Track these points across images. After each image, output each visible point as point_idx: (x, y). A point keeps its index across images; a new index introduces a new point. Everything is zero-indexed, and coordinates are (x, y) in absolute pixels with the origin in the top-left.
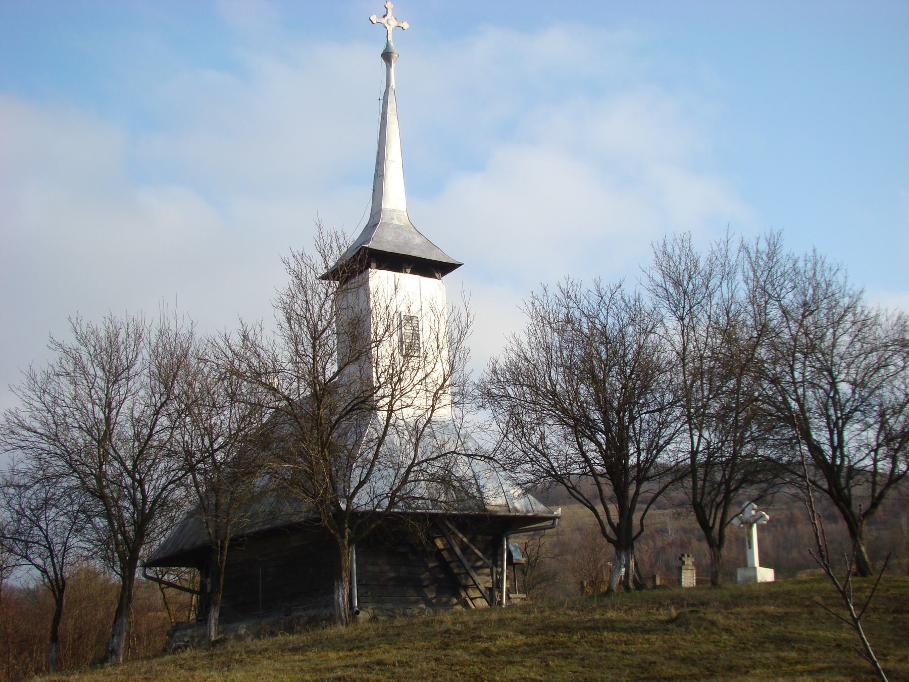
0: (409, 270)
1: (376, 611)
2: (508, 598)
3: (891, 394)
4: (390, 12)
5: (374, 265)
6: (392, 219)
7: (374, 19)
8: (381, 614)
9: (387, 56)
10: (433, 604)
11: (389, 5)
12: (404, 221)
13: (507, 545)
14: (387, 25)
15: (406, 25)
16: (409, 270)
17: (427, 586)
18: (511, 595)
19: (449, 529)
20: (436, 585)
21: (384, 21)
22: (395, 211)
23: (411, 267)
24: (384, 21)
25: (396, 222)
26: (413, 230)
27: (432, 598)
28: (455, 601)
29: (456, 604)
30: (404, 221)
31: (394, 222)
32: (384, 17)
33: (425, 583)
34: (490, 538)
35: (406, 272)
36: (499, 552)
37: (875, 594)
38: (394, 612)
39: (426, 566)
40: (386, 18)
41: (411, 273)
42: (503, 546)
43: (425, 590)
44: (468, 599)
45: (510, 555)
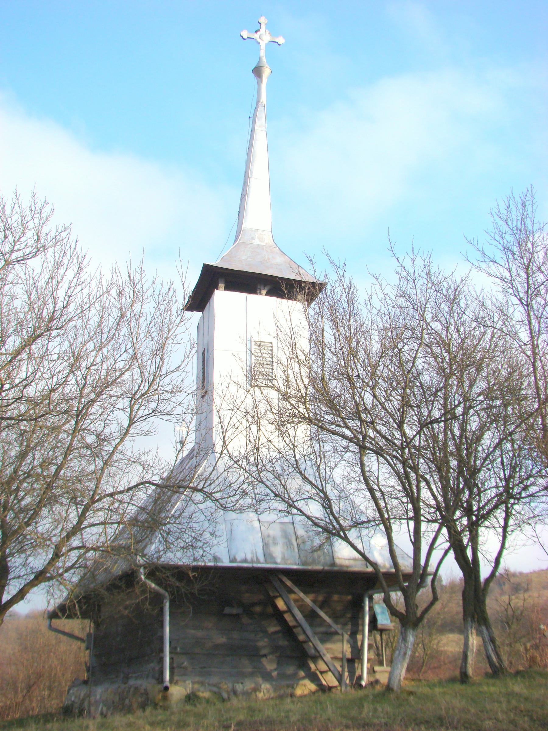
0: (264, 292)
1: (196, 686)
2: (372, 671)
3: (546, 243)
4: (263, 27)
5: (222, 286)
6: (253, 238)
7: (245, 34)
8: (202, 689)
9: (257, 71)
10: (272, 677)
11: (263, 20)
12: (268, 240)
13: (371, 608)
14: (259, 40)
15: (281, 40)
16: (264, 292)
17: (265, 656)
18: (377, 668)
19: (286, 586)
20: (278, 654)
21: (256, 36)
22: (257, 230)
23: (267, 288)
24: (256, 36)
25: (257, 241)
26: (276, 250)
27: (272, 671)
28: (302, 673)
29: (303, 678)
30: (268, 240)
31: (254, 242)
32: (256, 32)
33: (263, 652)
34: (349, 597)
35: (261, 294)
36: (360, 616)
37: (222, 456)
38: (220, 688)
39: (265, 632)
40: (259, 33)
41: (267, 294)
42: (362, 608)
43: (264, 660)
44: (318, 672)
45: (373, 620)
